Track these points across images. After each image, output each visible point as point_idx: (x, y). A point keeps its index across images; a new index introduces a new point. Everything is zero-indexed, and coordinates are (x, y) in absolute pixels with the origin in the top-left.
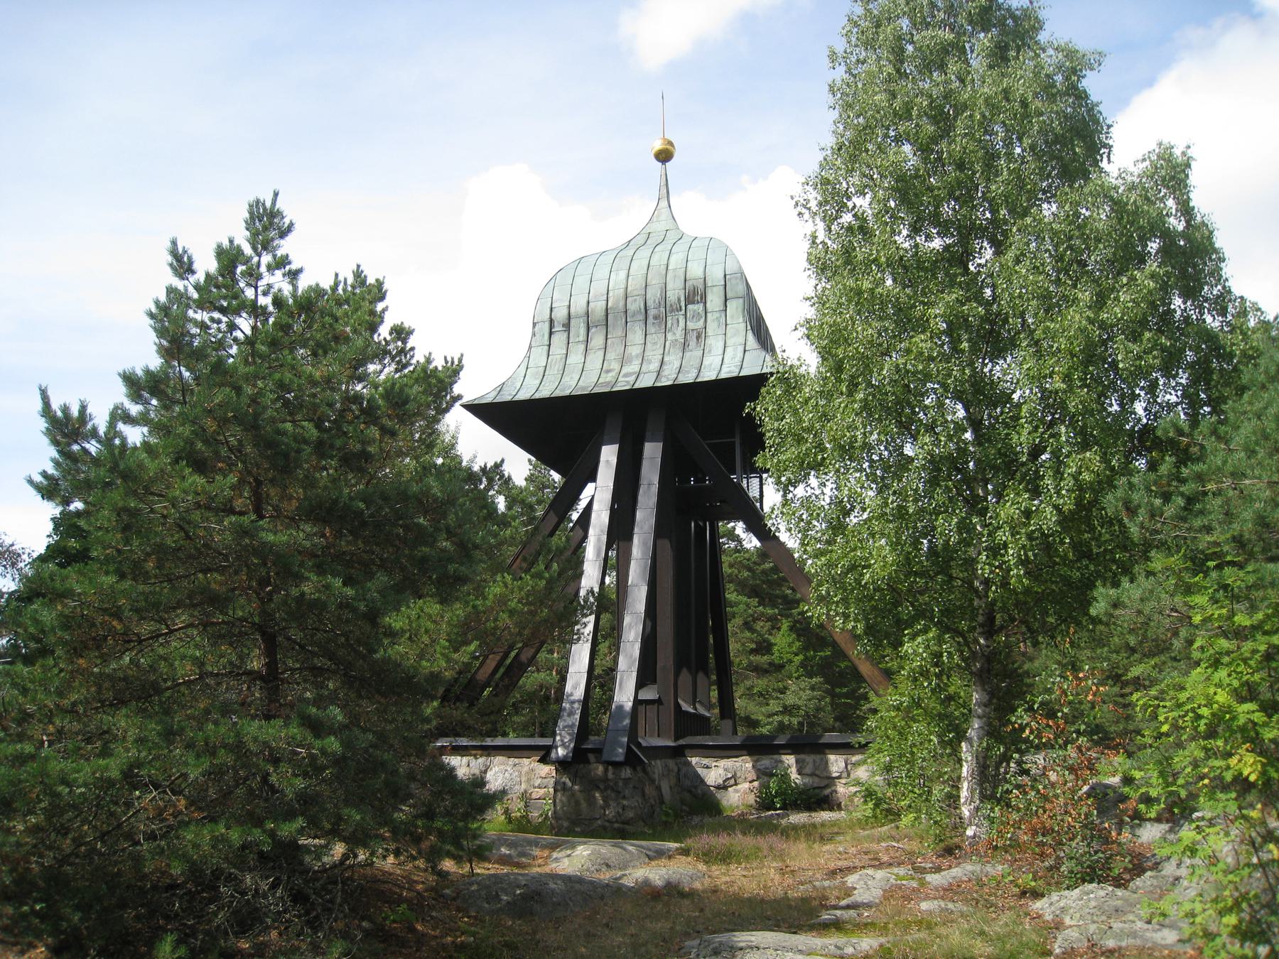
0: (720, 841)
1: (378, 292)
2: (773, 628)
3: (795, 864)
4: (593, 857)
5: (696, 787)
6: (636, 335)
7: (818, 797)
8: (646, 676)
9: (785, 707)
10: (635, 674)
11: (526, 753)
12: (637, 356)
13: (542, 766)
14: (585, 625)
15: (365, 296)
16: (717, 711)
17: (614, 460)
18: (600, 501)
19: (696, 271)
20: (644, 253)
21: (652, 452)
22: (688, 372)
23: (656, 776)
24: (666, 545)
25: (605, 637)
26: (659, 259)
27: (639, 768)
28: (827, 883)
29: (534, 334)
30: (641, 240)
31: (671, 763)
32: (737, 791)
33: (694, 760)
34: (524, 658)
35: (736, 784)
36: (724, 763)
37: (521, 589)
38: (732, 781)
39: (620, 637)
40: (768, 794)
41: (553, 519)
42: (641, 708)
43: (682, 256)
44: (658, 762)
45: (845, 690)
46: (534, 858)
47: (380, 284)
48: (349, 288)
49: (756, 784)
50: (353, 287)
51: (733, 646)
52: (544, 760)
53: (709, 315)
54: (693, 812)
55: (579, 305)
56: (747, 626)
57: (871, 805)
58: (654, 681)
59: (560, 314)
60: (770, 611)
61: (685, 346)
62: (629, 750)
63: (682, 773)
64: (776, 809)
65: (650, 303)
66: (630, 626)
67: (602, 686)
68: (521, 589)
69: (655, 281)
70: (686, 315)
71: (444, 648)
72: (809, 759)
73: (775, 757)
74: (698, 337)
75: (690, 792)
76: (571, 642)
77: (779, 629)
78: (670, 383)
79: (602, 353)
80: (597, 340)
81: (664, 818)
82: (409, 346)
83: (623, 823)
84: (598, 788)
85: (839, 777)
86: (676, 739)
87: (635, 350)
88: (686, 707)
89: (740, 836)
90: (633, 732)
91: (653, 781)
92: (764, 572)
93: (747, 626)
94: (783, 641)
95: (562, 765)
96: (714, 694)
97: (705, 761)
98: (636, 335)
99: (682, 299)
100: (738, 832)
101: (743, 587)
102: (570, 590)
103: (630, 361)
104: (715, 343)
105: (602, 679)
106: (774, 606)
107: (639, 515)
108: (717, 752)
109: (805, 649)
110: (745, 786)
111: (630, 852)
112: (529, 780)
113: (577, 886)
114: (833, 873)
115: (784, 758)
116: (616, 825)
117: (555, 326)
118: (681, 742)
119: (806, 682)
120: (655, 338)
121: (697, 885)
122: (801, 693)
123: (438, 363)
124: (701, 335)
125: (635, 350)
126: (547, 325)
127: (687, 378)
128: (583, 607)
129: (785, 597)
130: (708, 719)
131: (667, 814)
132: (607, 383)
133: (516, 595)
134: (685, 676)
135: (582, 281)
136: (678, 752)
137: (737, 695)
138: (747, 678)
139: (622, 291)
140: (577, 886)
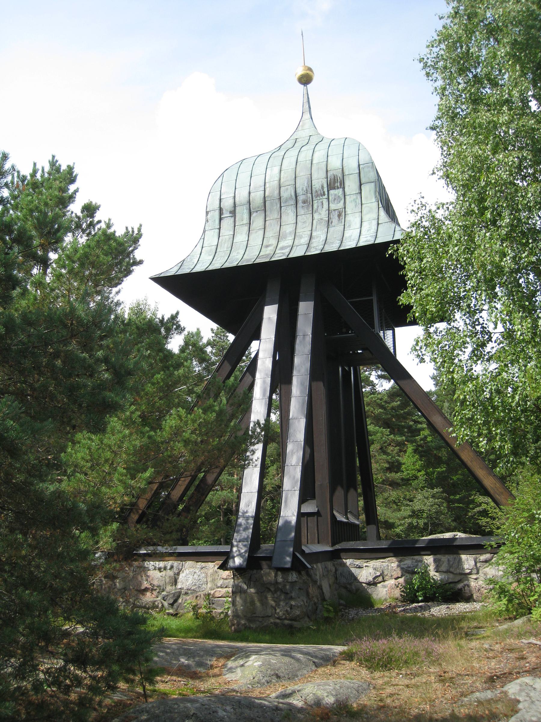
0: (380, 645)
1: (70, 177)
2: (400, 451)
3: (453, 669)
4: (263, 669)
5: (350, 584)
6: (289, 216)
7: (454, 592)
8: (307, 492)
9: (413, 512)
10: (297, 493)
11: (210, 558)
12: (290, 233)
13: (221, 572)
14: (253, 452)
15: (62, 179)
16: (363, 517)
17: (274, 317)
18: (265, 351)
19: (335, 163)
20: (293, 153)
21: (306, 309)
22: (332, 243)
23: (318, 577)
24: (320, 387)
25: (273, 463)
26: (305, 155)
27: (303, 573)
28: (489, 694)
29: (207, 221)
30: (290, 144)
31: (329, 565)
32: (385, 587)
33: (348, 562)
34: (210, 479)
35: (384, 581)
36: (373, 563)
37: (194, 421)
38: (380, 579)
39: (284, 462)
40: (412, 589)
41: (227, 367)
42: (304, 520)
43: (324, 153)
44: (319, 565)
45: (458, 497)
46: (212, 667)
47: (70, 169)
48: (46, 175)
49: (401, 580)
50: (49, 174)
51: (374, 466)
52: (223, 567)
53: (347, 197)
54: (350, 605)
55: (242, 196)
56: (383, 450)
57: (505, 601)
58: (313, 497)
59: (228, 204)
60: (399, 439)
61: (329, 223)
62: (294, 557)
63: (339, 572)
64: (418, 602)
65: (299, 191)
66: (292, 453)
67: (272, 500)
68: (194, 421)
69: (303, 175)
70: (328, 198)
71: (122, 475)
72: (445, 558)
73: (416, 557)
74: (339, 216)
75: (346, 588)
76: (243, 468)
77: (405, 452)
78: (318, 252)
79: (261, 232)
80: (258, 221)
81: (326, 615)
82: (96, 220)
83: (291, 620)
84: (269, 590)
85: (470, 573)
86: (333, 545)
87: (288, 229)
88: (340, 518)
89: (397, 638)
90: (297, 542)
91: (315, 582)
92: (393, 408)
93: (383, 450)
94: (409, 460)
95: (238, 571)
96: (361, 503)
97: (358, 562)
98: (289, 216)
99: (325, 186)
100: (394, 635)
101: (377, 420)
102: (243, 426)
103: (285, 237)
104: (353, 219)
105: (269, 496)
106: (402, 434)
107: (297, 360)
108: (367, 555)
109: (425, 467)
110: (391, 582)
111: (298, 660)
112: (213, 580)
113: (247, 712)
114: (492, 680)
115: (425, 557)
116: (286, 622)
117: (224, 214)
118: (338, 547)
119: (428, 492)
120: (305, 217)
121: (364, 700)
122: (425, 500)
123: (119, 231)
124: (342, 214)
125: (288, 229)
126: (217, 213)
127: (332, 247)
128: (252, 437)
129: (410, 427)
130: (358, 525)
131: (328, 611)
132: (267, 255)
133: (191, 427)
134: (340, 492)
135: (244, 178)
136: (335, 555)
137: (378, 502)
138: (384, 491)
139: (276, 183)
140: (247, 712)
